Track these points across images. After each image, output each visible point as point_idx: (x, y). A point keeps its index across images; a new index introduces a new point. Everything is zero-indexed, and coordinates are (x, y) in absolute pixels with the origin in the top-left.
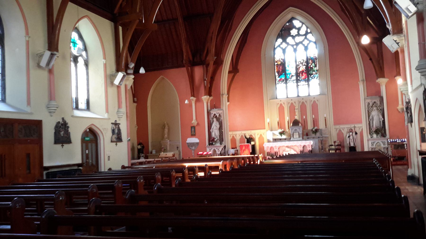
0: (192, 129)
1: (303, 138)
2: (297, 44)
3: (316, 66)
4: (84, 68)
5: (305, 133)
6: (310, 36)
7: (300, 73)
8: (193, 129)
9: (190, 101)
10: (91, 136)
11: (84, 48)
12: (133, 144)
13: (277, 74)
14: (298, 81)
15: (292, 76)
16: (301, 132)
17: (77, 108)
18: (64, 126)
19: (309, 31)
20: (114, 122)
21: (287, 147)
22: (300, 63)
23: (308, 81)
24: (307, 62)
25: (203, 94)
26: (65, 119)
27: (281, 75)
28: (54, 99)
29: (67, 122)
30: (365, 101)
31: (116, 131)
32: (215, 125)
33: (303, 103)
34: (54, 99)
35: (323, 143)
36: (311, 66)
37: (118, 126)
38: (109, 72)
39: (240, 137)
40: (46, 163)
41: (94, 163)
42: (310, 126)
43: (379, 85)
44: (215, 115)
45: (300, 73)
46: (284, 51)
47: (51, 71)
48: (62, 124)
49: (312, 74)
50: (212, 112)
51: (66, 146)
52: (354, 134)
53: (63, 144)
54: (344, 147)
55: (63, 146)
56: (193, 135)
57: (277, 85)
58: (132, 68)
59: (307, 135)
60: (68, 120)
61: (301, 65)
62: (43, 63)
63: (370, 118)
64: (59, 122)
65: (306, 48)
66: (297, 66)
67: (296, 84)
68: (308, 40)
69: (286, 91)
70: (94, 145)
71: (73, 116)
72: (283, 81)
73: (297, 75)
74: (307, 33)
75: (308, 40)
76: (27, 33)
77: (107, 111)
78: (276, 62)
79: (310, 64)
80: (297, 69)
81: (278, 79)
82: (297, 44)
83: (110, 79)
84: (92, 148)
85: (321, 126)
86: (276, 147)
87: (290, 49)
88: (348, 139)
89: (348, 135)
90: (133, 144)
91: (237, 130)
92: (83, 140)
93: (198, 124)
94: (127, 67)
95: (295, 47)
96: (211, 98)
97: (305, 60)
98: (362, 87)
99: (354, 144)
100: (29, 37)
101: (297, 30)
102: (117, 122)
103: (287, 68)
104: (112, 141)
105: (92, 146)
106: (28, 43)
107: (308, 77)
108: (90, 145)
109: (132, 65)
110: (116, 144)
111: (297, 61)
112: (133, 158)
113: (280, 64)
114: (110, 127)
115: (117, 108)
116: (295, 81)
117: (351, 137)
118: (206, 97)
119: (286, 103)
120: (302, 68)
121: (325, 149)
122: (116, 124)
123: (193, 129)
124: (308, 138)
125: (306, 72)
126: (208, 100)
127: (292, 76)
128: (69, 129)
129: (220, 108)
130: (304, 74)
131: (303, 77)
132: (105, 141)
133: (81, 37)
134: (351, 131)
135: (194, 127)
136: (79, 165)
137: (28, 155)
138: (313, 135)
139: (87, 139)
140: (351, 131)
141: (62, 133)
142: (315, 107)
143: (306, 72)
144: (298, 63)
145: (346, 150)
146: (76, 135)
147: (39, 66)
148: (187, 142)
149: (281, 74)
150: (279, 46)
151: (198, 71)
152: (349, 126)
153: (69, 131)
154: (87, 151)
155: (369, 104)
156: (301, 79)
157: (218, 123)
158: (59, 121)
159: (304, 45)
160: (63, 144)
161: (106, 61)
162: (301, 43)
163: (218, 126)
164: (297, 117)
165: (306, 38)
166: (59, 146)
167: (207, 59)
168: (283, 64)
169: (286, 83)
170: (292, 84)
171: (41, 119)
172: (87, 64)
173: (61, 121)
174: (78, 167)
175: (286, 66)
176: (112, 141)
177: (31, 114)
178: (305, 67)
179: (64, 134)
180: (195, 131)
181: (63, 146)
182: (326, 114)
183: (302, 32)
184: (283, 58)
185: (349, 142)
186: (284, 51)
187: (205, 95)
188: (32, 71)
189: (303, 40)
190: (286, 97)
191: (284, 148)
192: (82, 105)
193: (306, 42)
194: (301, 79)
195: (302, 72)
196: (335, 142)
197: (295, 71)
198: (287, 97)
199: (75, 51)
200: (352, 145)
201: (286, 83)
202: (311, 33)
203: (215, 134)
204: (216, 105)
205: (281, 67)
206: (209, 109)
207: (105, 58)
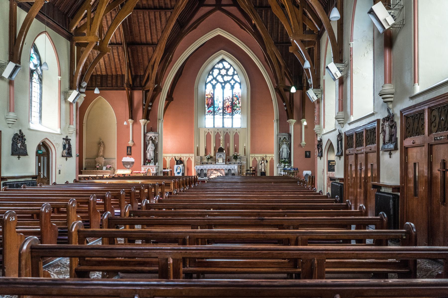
0: (128, 149)
1: (226, 163)
2: (225, 82)
3: (239, 103)
6: (236, 77)
8: (129, 149)
9: (128, 122)
10: (44, 151)
13: (206, 106)
14: (224, 113)
15: (219, 109)
16: (225, 158)
19: (236, 73)
20: (65, 138)
21: (215, 170)
23: (232, 115)
24: (233, 99)
25: (141, 117)
26: (23, 131)
27: (210, 107)
30: (277, 136)
31: (67, 146)
32: (151, 147)
33: (227, 133)
35: (242, 168)
37: (69, 141)
38: (62, 89)
39: (170, 159)
42: (232, 153)
43: (288, 125)
44: (151, 137)
45: (226, 108)
46: (214, 87)
50: (148, 134)
51: (22, 158)
52: (265, 162)
54: (257, 172)
55: (19, 157)
57: (206, 116)
58: (85, 87)
59: (229, 161)
60: (25, 132)
61: (227, 101)
63: (281, 150)
64: (17, 134)
65: (232, 87)
66: (224, 101)
67: (222, 117)
68: (234, 80)
69: (210, 122)
70: (45, 158)
72: (212, 112)
73: (224, 109)
74: (234, 74)
75: (234, 80)
78: (207, 95)
80: (224, 104)
81: (207, 110)
82: (225, 82)
83: (64, 95)
84: (44, 162)
85: (241, 153)
86: (205, 169)
87: (219, 86)
88: (260, 166)
92: (37, 154)
93: (134, 145)
94: (80, 86)
95: (223, 84)
96: (149, 121)
97: (231, 97)
98: (275, 125)
101: (226, 71)
102: (69, 138)
103: (216, 102)
104: (63, 156)
107: (232, 112)
108: (42, 158)
109: (85, 84)
110: (66, 159)
111: (225, 97)
112: (80, 173)
114: (61, 142)
115: (68, 125)
116: (221, 114)
117: (263, 165)
118: (143, 120)
119: (222, 132)
120: (228, 103)
121: (243, 173)
122: (67, 140)
123: (129, 149)
124: (230, 163)
125: (231, 108)
126: (145, 124)
127: (219, 109)
129: (156, 132)
131: (229, 111)
134: (263, 159)
135: (130, 147)
138: (234, 161)
139: (40, 152)
141: (19, 145)
142: (236, 137)
143: (231, 108)
145: (259, 174)
148: (123, 161)
149: (210, 107)
150: (210, 82)
151: (138, 95)
152: (262, 155)
155: (280, 138)
157: (153, 145)
158: (16, 133)
159: (231, 84)
162: (228, 82)
163: (154, 148)
164: (221, 146)
165: (233, 78)
166: (15, 158)
167: (147, 85)
168: (212, 98)
169: (214, 115)
170: (218, 118)
172: (40, 79)
175: (215, 99)
176: (63, 156)
178: (230, 103)
180: (131, 151)
181: (19, 157)
182: (245, 144)
183: (231, 72)
184: (213, 93)
185: (261, 168)
186: (214, 87)
187: (143, 119)
189: (231, 80)
190: (213, 126)
191: (212, 171)
193: (232, 82)
195: (228, 107)
196: (251, 168)
197: (222, 106)
198: (223, 127)
200: (263, 170)
201: (214, 115)
202: (237, 74)
203: (150, 155)
204: (152, 128)
206: (146, 131)
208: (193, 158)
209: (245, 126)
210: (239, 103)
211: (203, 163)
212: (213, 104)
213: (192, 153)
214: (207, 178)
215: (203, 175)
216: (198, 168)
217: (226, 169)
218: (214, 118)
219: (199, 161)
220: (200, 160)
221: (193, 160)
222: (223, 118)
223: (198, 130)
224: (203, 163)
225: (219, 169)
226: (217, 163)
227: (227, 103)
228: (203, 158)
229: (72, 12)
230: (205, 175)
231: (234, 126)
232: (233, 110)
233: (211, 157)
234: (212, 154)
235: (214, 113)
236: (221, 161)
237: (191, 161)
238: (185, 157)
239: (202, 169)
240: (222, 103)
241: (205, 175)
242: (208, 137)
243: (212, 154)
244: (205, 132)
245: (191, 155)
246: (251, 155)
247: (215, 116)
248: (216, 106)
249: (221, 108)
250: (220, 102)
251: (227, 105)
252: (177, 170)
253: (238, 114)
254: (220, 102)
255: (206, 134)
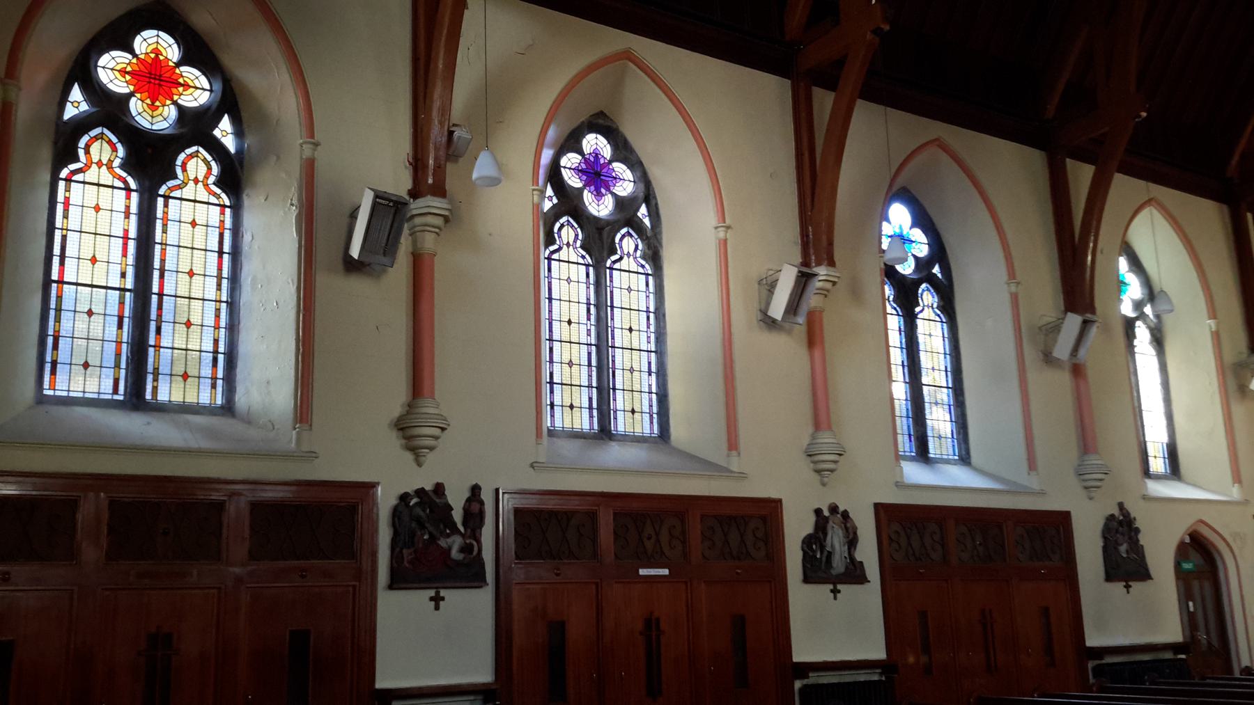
4: (1151, 351)
10: (1201, 557)
11: (1146, 291)
17: (1147, 473)
18: (1126, 528)
26: (1127, 506)
28: (1096, 452)
29: (1132, 515)
34: (1096, 452)
38: (1229, 358)
40: (1093, 640)
41: (1215, 642)
47: (1077, 371)
48: (1120, 523)
51: (1136, 586)
53: (835, 584)
55: (1128, 587)
62: (1062, 350)
64: (1112, 515)
70: (1207, 585)
71: (1147, 498)
76: (1012, 274)
77: (1237, 478)
100: (1018, 283)
105: (1201, 588)
106: (1015, 298)
108: (1196, 584)
110: (437, 600)
128: (1140, 536)
132: (1242, 571)
133: (1136, 265)
136: (1175, 647)
137: (1045, 612)
139: (1187, 566)
146: (1160, 552)
147: (1048, 358)
153: (1142, 542)
154: (1191, 604)
160: (835, 584)
161: (1218, 325)
166: (1119, 587)
171: (774, 495)
172: (1158, 340)
173: (1116, 512)
174: (1176, 653)
177: (1042, 493)
179: (1127, 552)
181: (1128, 587)
188: (1032, 376)
192: (1158, 464)
199: (1127, 309)
207: (1213, 314)
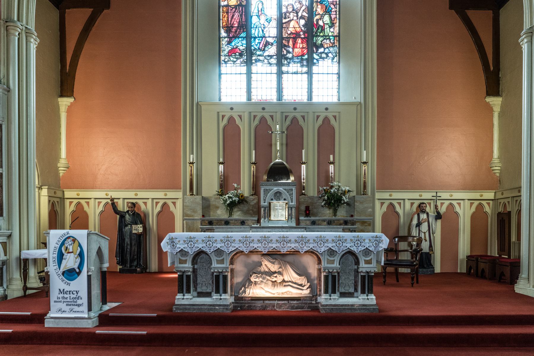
1: (298, 222)
5: (303, 208)
7: (288, 39)
12: (386, 311)
13: (223, 34)
14: (281, 59)
15: (267, 44)
22: (290, 10)
23: (310, 63)
24: (310, 10)
27: (236, 37)
36: (321, 23)
45: (288, 39)
49: (322, 46)
56: (304, 190)
57: (223, 65)
59: (308, 212)
66: (281, 16)
67: (274, 69)
72: (241, 55)
79: (318, 17)
80: (281, 26)
81: (226, 49)
86: (219, 252)
89: (415, 222)
90: (386, 311)
91: (92, 187)
99: (431, 246)
103: (254, 20)
107: (311, 53)
113: (236, 7)
116: (274, 61)
117: (424, 227)
119: (278, 117)
120: (296, 25)
124: (314, 223)
127: (267, 44)
130: (299, 41)
131: (297, 51)
140: (421, 208)
142: (327, 133)
144: (284, 10)
152: (416, 195)
156: (290, 56)
169: (249, 63)
178: (302, 22)
191: (255, 258)
194: (290, 56)
195: (296, 36)
201: (249, 63)
205: (236, 15)
208: (179, 203)
209: (355, 95)
210: (332, 25)
211: (211, 223)
212: (245, 26)
213: (175, 187)
214: (228, 299)
215: (205, 282)
216: (181, 246)
217: (331, 252)
218: (249, 74)
219: (198, 216)
220: (200, 212)
221: (178, 212)
222: (280, 74)
223: (197, 109)
224: (211, 223)
225: (295, 253)
226: (264, 222)
227: (292, 24)
228: (213, 202)
229: (287, 284)
230: (220, 283)
231: (315, 100)
232: (312, 46)
233: (242, 200)
234: (245, 190)
235: (249, 57)
236: (280, 213)
237: (172, 217)
238: (149, 202)
239: (200, 253)
240: (274, 23)
241: (220, 283)
242: (230, 133)
243: (245, 190)
244: (220, 117)
245: (171, 194)
246: (378, 195)
247: (254, 68)
248: (254, 32)
249: (270, 40)
250: (269, 21)
251: (291, 30)
252: (61, 257)
253: (328, 62)
254: (269, 21)
255: (222, 125)
